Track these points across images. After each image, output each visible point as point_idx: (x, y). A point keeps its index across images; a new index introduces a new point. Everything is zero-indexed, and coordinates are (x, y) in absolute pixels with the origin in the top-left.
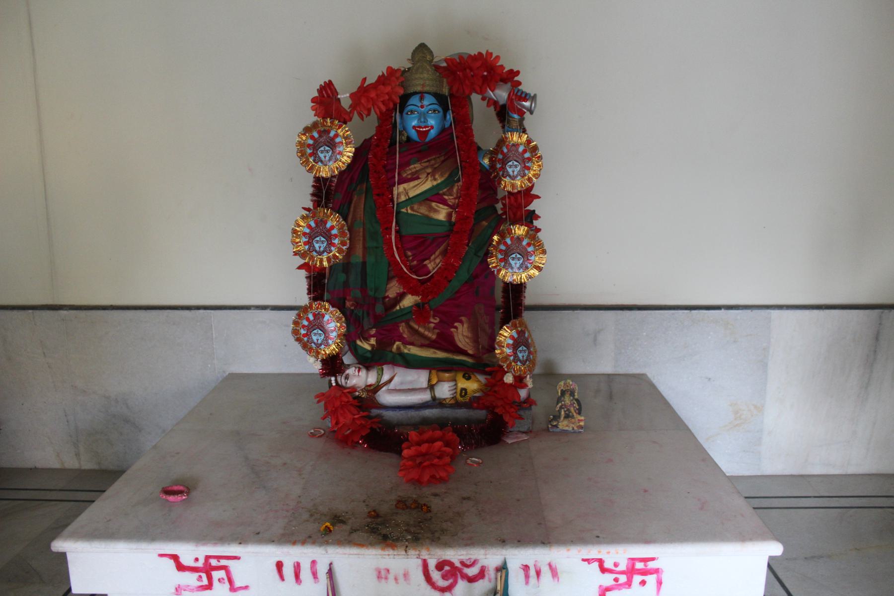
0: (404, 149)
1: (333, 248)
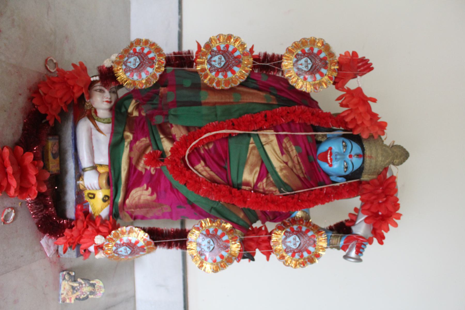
0: (310, 139)
1: (214, 73)
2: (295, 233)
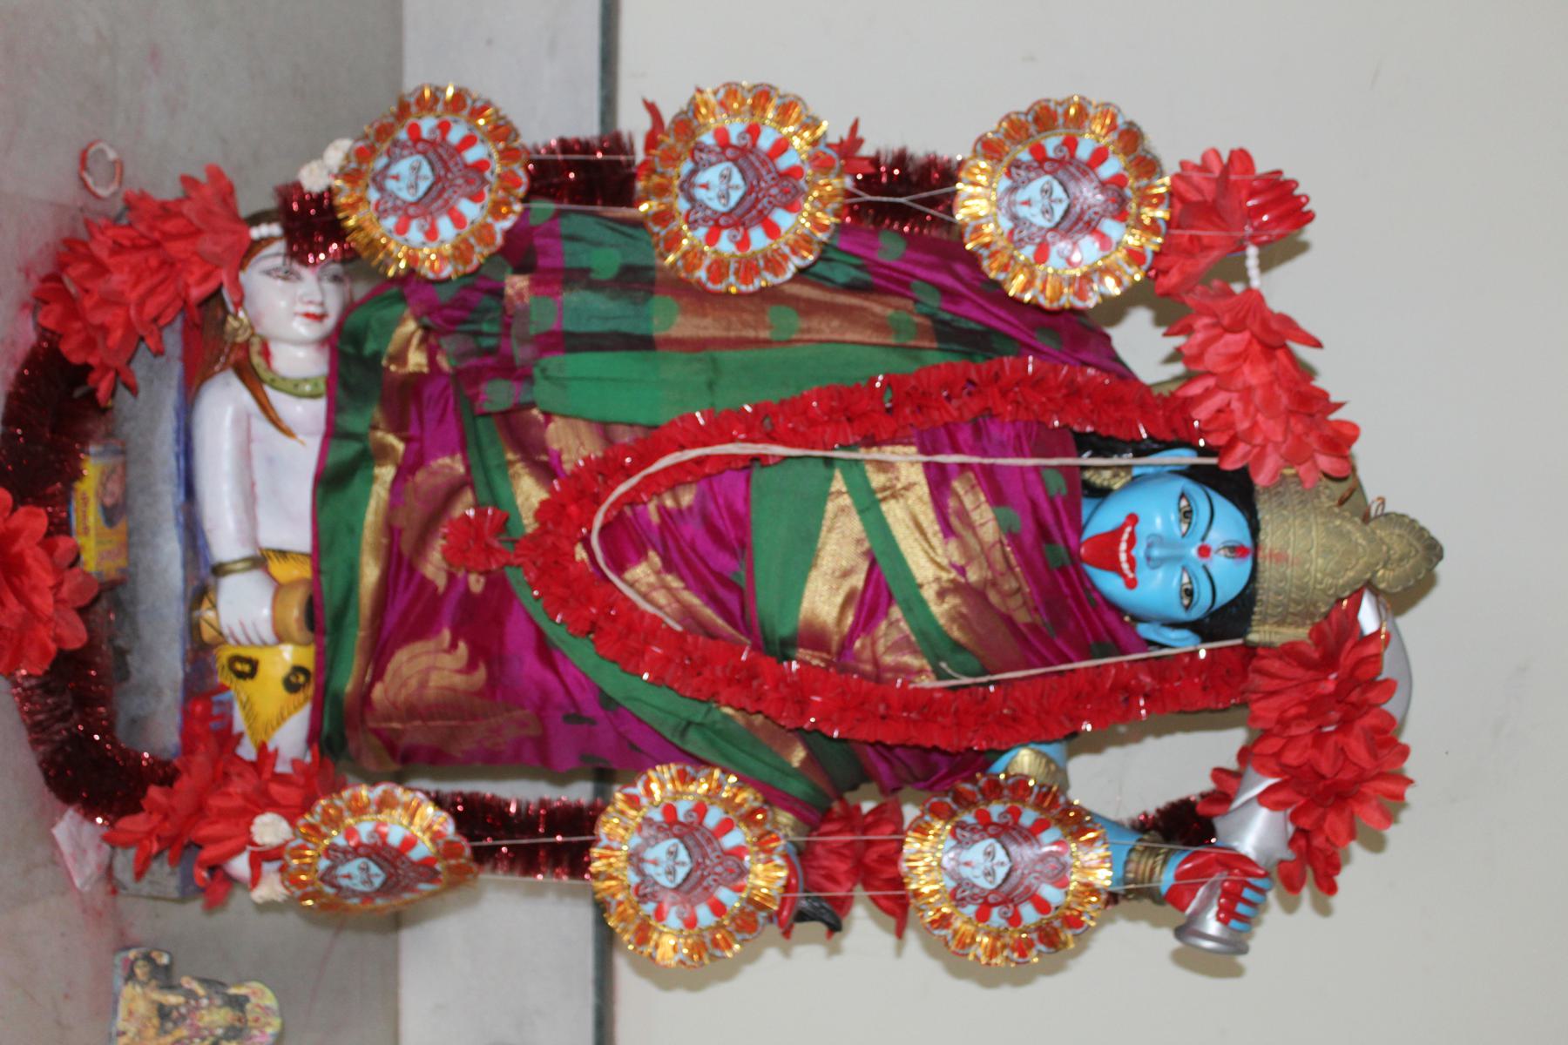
2: (991, 830)
